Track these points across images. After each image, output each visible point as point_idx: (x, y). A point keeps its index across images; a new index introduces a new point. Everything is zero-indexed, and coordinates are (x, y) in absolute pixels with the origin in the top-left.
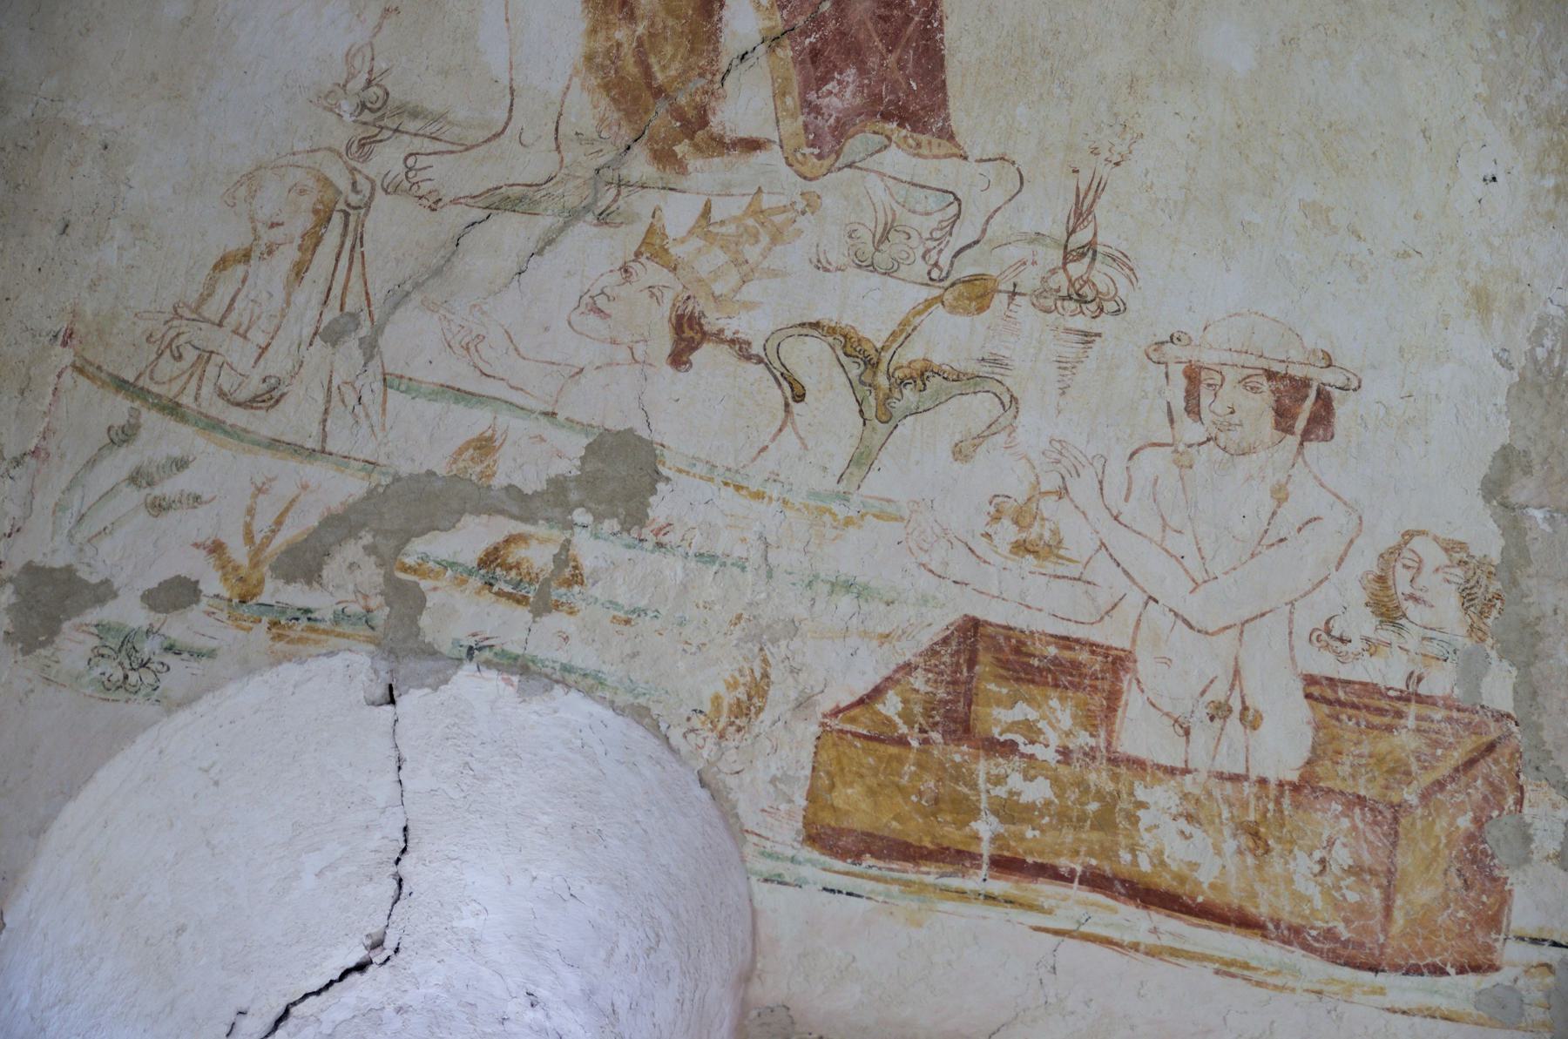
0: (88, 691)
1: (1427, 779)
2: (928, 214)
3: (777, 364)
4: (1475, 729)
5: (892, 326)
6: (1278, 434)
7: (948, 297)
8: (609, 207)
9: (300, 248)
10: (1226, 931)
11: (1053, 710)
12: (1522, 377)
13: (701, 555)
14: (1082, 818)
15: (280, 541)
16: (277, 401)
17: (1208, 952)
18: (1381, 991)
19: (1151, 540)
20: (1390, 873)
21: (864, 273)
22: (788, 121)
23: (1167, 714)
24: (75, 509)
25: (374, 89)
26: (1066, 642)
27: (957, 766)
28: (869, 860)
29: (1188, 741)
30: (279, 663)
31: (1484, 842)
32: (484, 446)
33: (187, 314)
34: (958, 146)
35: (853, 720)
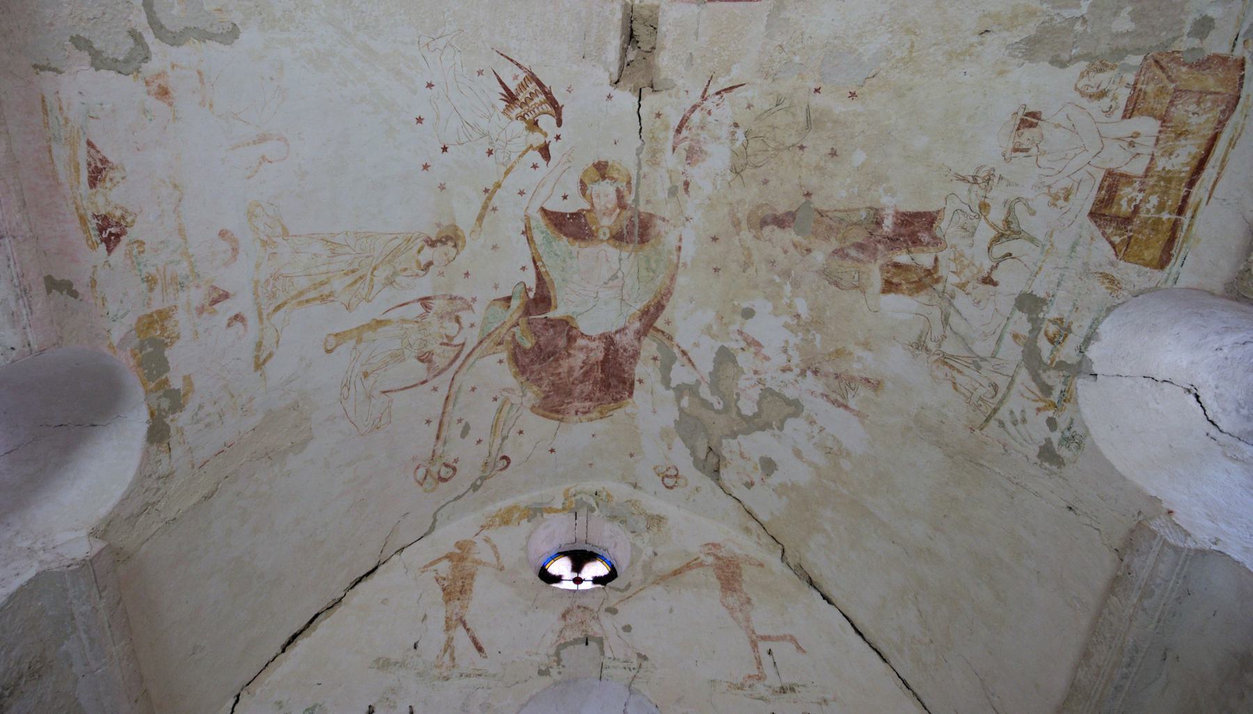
1: (1166, 81)
4: (1149, 66)
12: (1027, 59)
14: (1166, 187)
20: (1201, 92)
26: (1100, 188)
27: (1141, 222)
28: (1173, 252)
30: (1077, 403)
32: (1016, 337)
35: (1120, 251)
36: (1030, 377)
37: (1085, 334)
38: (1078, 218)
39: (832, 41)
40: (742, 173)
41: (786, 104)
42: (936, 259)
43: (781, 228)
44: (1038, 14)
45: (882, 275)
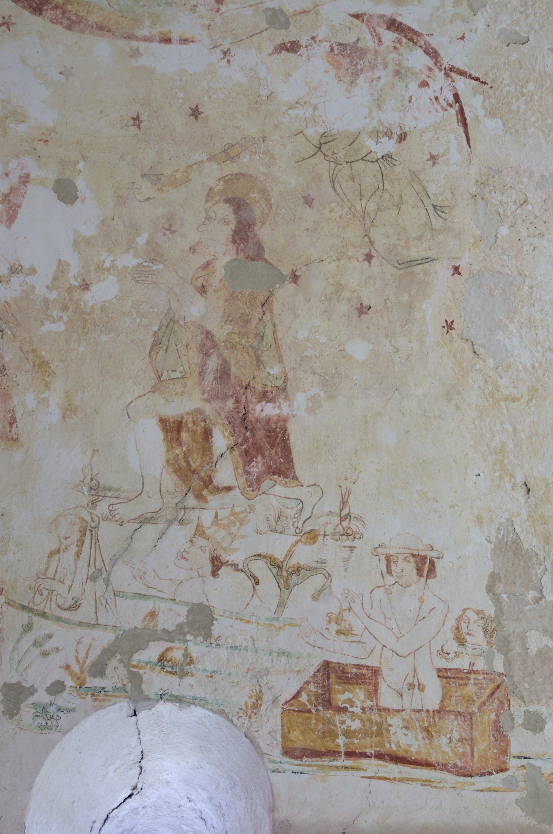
0: (35, 731)
1: (479, 702)
2: (292, 508)
3: (248, 572)
4: (492, 681)
5: (285, 552)
6: (418, 577)
7: (303, 539)
8: (182, 518)
9: (77, 545)
10: (422, 769)
11: (357, 693)
12: (495, 546)
13: (232, 647)
14: (372, 733)
15: (89, 662)
16: (79, 607)
17: (418, 777)
18: (473, 784)
19: (381, 624)
20: (472, 739)
21: (273, 533)
22: (240, 478)
23: (394, 690)
24: (16, 659)
25: (94, 481)
26: (358, 666)
27: (329, 719)
28: (305, 759)
29: (402, 699)
30: (98, 710)
31: (500, 723)
32: (153, 615)
33: (42, 577)
34: (299, 482)
35: (292, 705)
36: (106, 646)
37: (184, 694)
38: (319, 650)
39: (527, 283)
40: (319, 157)
41: (437, 223)
42: (229, 489)
43: (233, 239)
44: (547, 548)
45: (188, 414)
